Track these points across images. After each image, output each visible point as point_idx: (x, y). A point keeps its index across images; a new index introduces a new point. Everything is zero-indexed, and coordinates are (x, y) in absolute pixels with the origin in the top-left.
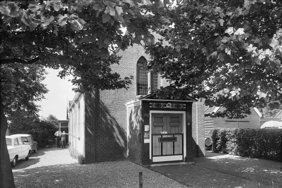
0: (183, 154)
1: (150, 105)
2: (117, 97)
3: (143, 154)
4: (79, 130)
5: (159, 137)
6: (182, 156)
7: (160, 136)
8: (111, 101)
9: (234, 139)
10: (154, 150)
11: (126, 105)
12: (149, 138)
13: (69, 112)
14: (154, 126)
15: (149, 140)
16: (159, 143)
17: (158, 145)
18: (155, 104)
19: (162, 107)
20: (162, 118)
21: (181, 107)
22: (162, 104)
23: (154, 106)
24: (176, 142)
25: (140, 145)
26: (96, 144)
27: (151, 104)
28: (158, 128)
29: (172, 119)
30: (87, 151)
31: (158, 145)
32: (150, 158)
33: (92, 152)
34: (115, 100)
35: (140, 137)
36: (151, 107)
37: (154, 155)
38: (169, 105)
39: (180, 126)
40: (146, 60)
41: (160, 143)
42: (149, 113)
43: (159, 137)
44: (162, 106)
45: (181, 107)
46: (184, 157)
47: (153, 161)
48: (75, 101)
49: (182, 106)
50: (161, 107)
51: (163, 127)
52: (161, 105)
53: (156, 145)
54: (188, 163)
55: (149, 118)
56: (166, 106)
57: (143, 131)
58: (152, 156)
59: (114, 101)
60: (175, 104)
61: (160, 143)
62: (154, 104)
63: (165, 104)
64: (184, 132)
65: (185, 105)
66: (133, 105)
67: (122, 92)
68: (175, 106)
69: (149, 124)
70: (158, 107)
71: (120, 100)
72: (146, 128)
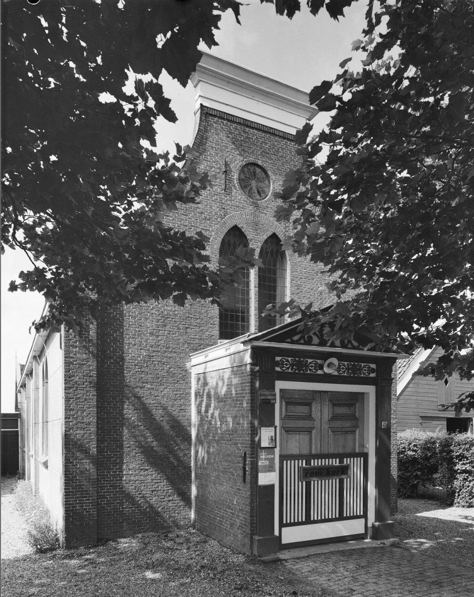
0: (365, 516)
1: (278, 364)
2: (162, 342)
3: (254, 520)
4: (45, 439)
5: (300, 465)
6: (363, 520)
7: (304, 461)
8: (144, 354)
9: (463, 464)
10: (287, 503)
11: (188, 365)
12: (270, 469)
13: (21, 393)
14: (286, 431)
15: (273, 474)
16: (300, 483)
17: (294, 490)
18: (290, 359)
19: (310, 370)
20: (309, 405)
21: (364, 374)
22: (310, 363)
23: (288, 368)
24: (349, 479)
25: (246, 491)
26: (98, 484)
27: (278, 359)
28: (298, 436)
29: (291, 408)
30: (70, 507)
31: (294, 490)
32: (277, 533)
33: (86, 509)
34: (155, 349)
35: (245, 464)
36: (278, 369)
37: (285, 522)
38: (329, 365)
39: (357, 431)
40: (246, 237)
41: (302, 483)
42: (273, 388)
43: (300, 465)
44: (312, 366)
45: (364, 374)
46: (370, 525)
47: (285, 540)
48: (35, 357)
49: (365, 370)
50: (309, 372)
51: (311, 432)
52: (308, 366)
53: (290, 490)
54: (384, 543)
55: (273, 405)
56: (321, 367)
57: (254, 448)
58: (282, 525)
59: (154, 354)
60: (346, 363)
61: (302, 483)
62: (287, 361)
63: (319, 362)
64: (371, 447)
65: (373, 366)
66: (226, 363)
67: (179, 329)
68: (348, 369)
69: (271, 424)
70: (299, 371)
71: (170, 350)
72: (266, 436)
